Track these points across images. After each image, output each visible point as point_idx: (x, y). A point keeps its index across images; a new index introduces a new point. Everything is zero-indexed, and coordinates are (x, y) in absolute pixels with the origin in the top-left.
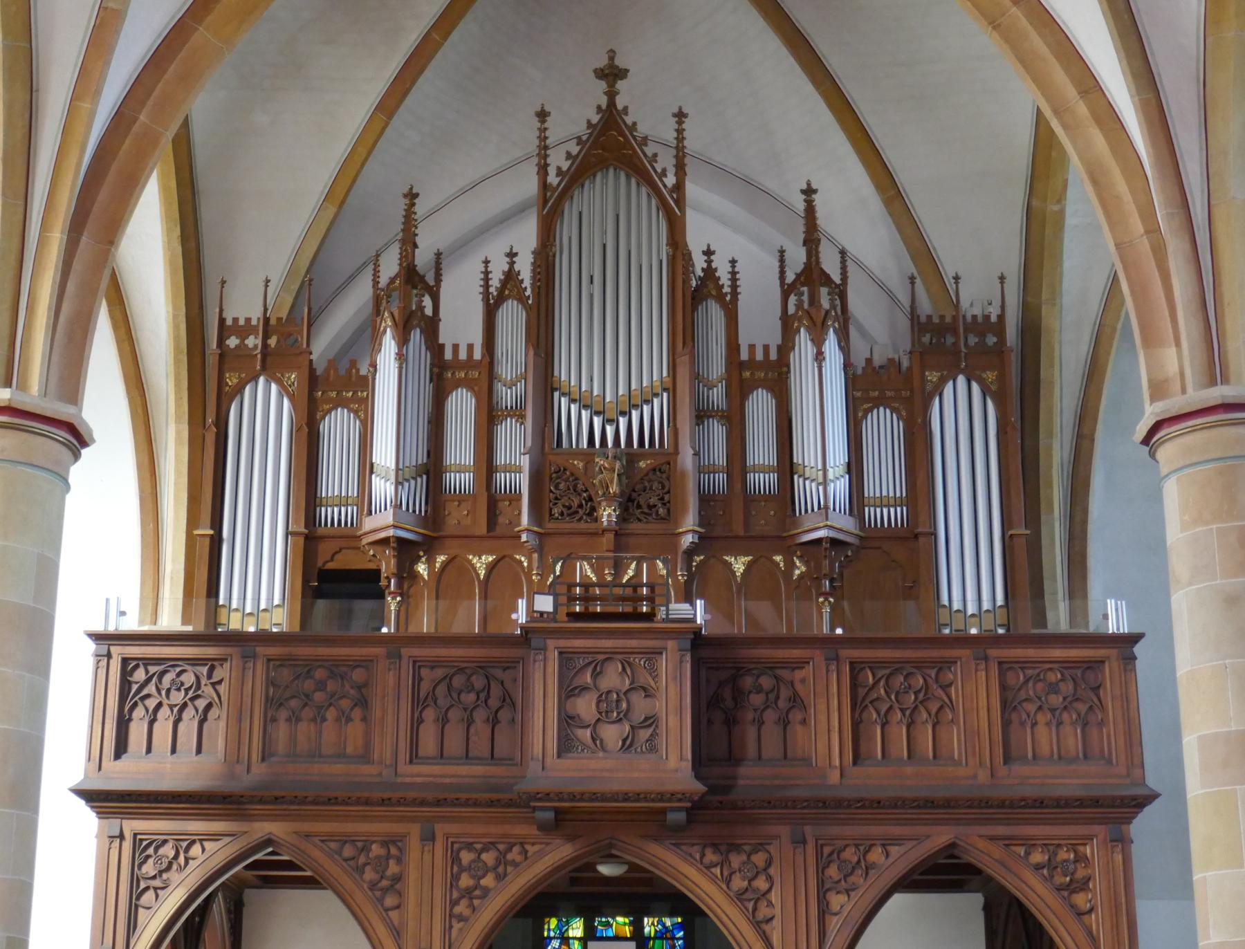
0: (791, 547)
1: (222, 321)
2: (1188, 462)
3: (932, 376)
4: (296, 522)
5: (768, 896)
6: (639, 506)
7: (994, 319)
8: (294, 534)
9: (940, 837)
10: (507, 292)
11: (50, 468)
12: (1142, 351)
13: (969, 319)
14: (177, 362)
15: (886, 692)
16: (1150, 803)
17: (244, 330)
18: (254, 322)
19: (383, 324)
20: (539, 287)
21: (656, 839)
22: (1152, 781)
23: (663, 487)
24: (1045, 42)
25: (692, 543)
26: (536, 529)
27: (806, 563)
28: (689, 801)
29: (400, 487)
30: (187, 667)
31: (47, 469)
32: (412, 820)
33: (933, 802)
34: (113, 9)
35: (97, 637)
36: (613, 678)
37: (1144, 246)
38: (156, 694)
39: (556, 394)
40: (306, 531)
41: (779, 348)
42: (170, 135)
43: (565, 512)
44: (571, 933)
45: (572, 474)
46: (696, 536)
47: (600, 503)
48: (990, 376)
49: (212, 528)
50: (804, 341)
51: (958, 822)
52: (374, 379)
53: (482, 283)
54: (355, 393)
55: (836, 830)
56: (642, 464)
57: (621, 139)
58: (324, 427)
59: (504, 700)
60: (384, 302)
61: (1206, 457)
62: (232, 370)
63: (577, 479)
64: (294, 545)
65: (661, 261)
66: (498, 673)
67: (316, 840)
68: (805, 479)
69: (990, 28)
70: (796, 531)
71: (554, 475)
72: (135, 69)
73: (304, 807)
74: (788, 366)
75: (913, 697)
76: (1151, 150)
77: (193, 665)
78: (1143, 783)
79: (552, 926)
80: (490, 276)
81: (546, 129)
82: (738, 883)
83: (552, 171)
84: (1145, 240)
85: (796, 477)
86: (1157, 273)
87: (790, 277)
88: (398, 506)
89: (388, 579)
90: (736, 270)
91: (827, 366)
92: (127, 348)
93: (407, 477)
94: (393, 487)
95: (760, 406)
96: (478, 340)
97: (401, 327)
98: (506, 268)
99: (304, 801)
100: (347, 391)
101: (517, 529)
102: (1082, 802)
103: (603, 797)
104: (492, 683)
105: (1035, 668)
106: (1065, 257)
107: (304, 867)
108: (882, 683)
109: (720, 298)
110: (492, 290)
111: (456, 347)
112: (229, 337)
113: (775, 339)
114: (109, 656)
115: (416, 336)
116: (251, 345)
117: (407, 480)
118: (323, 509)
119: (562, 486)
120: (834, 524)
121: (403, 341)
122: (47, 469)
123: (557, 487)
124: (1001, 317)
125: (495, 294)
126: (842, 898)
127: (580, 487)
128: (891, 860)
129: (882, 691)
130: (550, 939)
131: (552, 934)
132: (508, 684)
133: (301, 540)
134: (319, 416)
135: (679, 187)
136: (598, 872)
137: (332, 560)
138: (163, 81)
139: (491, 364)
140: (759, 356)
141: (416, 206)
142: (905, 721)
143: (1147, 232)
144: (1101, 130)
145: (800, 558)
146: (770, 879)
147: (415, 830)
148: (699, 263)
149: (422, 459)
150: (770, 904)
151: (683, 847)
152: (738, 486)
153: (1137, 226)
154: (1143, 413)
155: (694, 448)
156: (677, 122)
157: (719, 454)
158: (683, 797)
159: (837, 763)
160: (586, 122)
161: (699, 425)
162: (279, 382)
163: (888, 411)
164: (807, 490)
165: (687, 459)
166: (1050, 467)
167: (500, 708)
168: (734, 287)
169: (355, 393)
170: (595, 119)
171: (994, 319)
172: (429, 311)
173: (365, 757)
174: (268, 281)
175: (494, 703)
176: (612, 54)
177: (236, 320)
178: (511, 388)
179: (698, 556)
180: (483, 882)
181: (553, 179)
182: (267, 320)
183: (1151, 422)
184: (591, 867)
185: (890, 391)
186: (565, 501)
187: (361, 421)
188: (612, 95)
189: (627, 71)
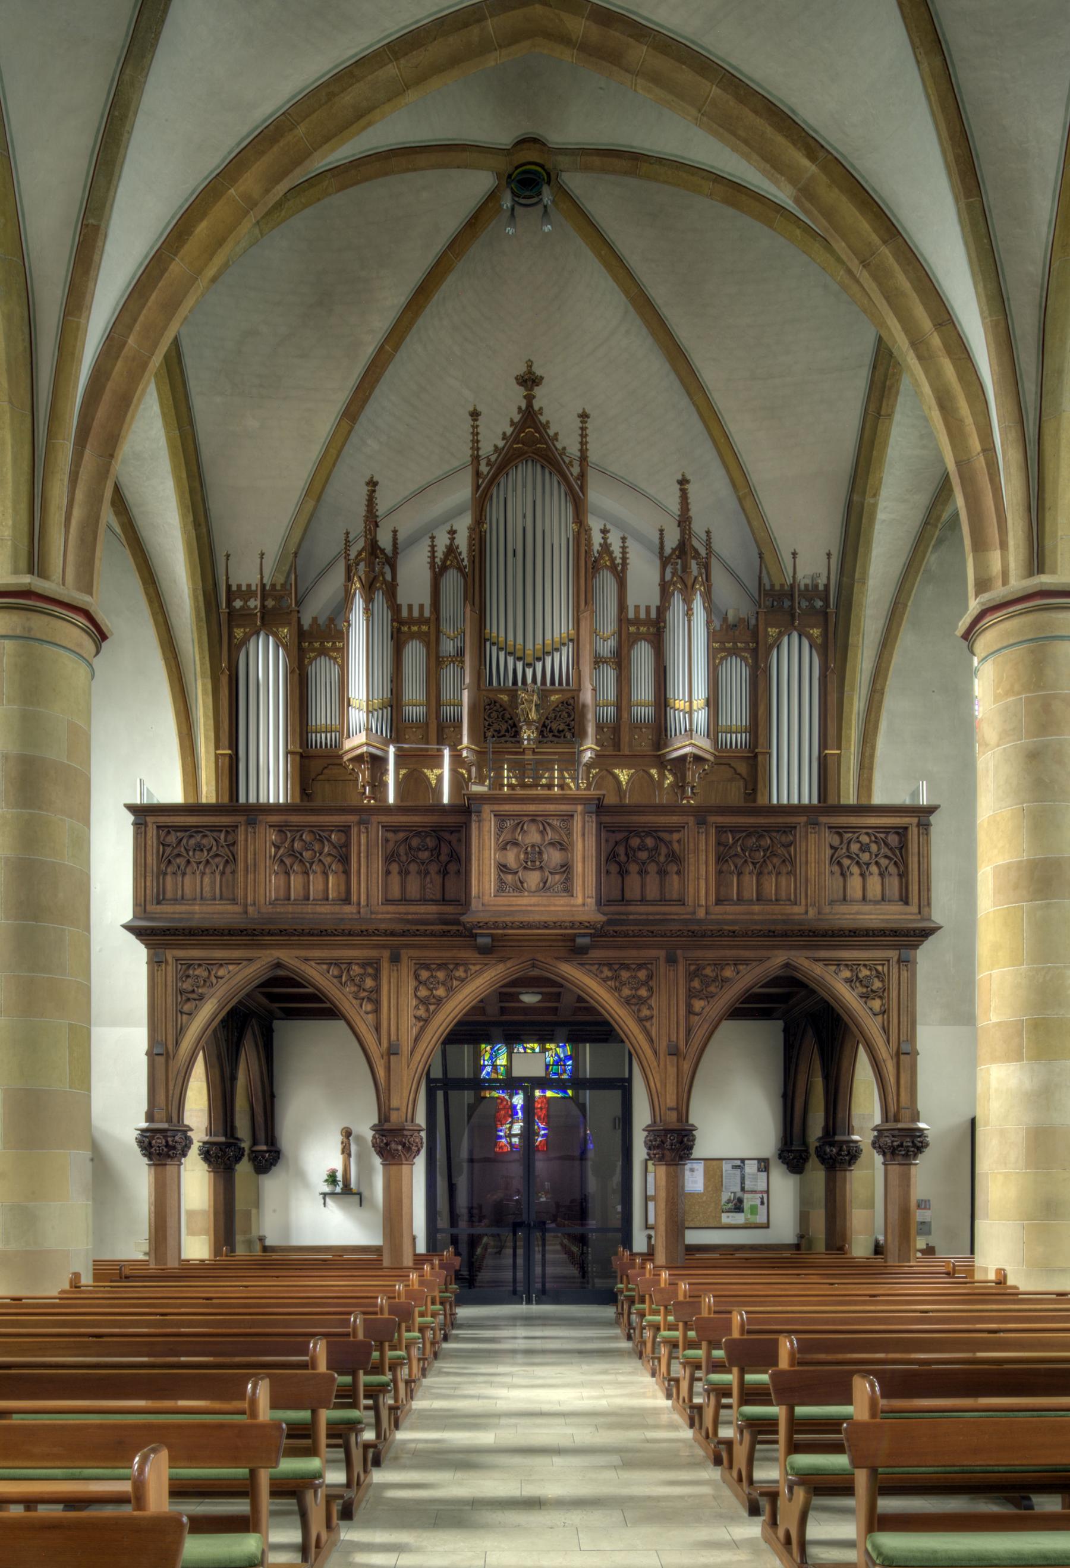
0: (661, 763)
1: (229, 587)
2: (1005, 644)
3: (773, 631)
4: (293, 742)
5: (649, 1001)
6: (551, 731)
7: (821, 588)
8: (293, 753)
9: (778, 959)
10: (449, 563)
11: (73, 648)
12: (971, 555)
13: (802, 587)
14: (199, 628)
15: (742, 849)
16: (933, 933)
17: (249, 594)
18: (254, 588)
19: (354, 587)
20: (474, 556)
21: (566, 960)
22: (938, 915)
23: (569, 716)
24: (908, 278)
25: (591, 758)
26: (473, 747)
27: (674, 775)
28: (594, 929)
29: (370, 715)
30: (208, 833)
31: (69, 649)
32: (384, 947)
33: (774, 932)
34: (94, 226)
35: (132, 808)
36: (533, 836)
37: (981, 462)
38: (185, 855)
39: (488, 644)
40: (301, 751)
41: (658, 608)
42: (157, 360)
43: (496, 734)
44: (498, 1062)
45: (501, 706)
46: (594, 753)
47: (521, 728)
48: (816, 632)
49: (230, 748)
50: (677, 604)
51: (791, 948)
52: (348, 632)
53: (429, 554)
54: (334, 643)
55: (699, 953)
56: (553, 698)
57: (537, 435)
58: (312, 670)
59: (452, 856)
60: (354, 568)
61: (1025, 638)
62: (239, 626)
63: (504, 710)
64: (293, 761)
65: (568, 539)
66: (446, 836)
67: (312, 963)
68: (675, 710)
69: (861, 266)
70: (667, 750)
71: (487, 707)
72: (122, 296)
73: (302, 938)
74: (665, 622)
75: (762, 854)
76: (996, 368)
77: (211, 831)
78: (929, 919)
79: (486, 1058)
80: (436, 549)
81: (477, 426)
82: (626, 992)
83: (483, 463)
84: (982, 458)
85: (668, 709)
86: (989, 486)
87: (668, 551)
88: (368, 729)
89: (364, 787)
90: (626, 545)
91: (694, 618)
92: (161, 619)
93: (376, 707)
94: (365, 714)
95: (642, 656)
96: (427, 602)
97: (367, 587)
98: (448, 542)
99: (302, 933)
100: (328, 642)
101: (459, 747)
102: (882, 933)
103: (529, 926)
104: (442, 844)
105: (854, 833)
106: (874, 545)
107: (307, 985)
108: (740, 842)
109: (613, 568)
110: (437, 560)
111: (410, 607)
112: (235, 600)
113: (655, 601)
114: (146, 824)
115: (379, 597)
116: (252, 606)
117: (376, 710)
118: (314, 735)
119: (494, 715)
120: (696, 743)
121: (369, 600)
122: (69, 649)
123: (489, 716)
124: (827, 586)
125: (440, 563)
126: (702, 1003)
127: (507, 716)
128: (740, 975)
129: (739, 849)
130: (485, 1066)
131: (486, 1063)
132: (454, 843)
133: (298, 758)
134: (306, 661)
135: (582, 476)
136: (522, 1002)
137: (322, 774)
138: (146, 308)
139: (438, 619)
140: (643, 615)
141: (377, 493)
142: (755, 872)
143: (984, 450)
144: (951, 358)
145: (670, 771)
146: (650, 989)
147: (386, 954)
148: (597, 539)
149: (387, 695)
150: (650, 1008)
151: (587, 967)
152: (625, 715)
153: (975, 444)
154: (966, 608)
155: (592, 685)
156: (582, 422)
157: (609, 692)
158: (589, 925)
159: (703, 903)
160: (509, 420)
161: (595, 668)
162: (275, 635)
163: (739, 660)
164: (678, 719)
165: (587, 696)
166: (851, 712)
167: (450, 861)
168: (624, 559)
169: (334, 643)
170: (517, 418)
171: (821, 588)
172: (389, 578)
173: (347, 900)
174: (262, 555)
175: (444, 858)
176: (530, 363)
177: (239, 586)
178: (453, 640)
179: (594, 769)
180: (437, 993)
181: (484, 469)
182: (263, 586)
183: (976, 612)
184: (514, 997)
185: (741, 642)
186: (496, 726)
187: (339, 666)
188: (529, 399)
189: (542, 378)
